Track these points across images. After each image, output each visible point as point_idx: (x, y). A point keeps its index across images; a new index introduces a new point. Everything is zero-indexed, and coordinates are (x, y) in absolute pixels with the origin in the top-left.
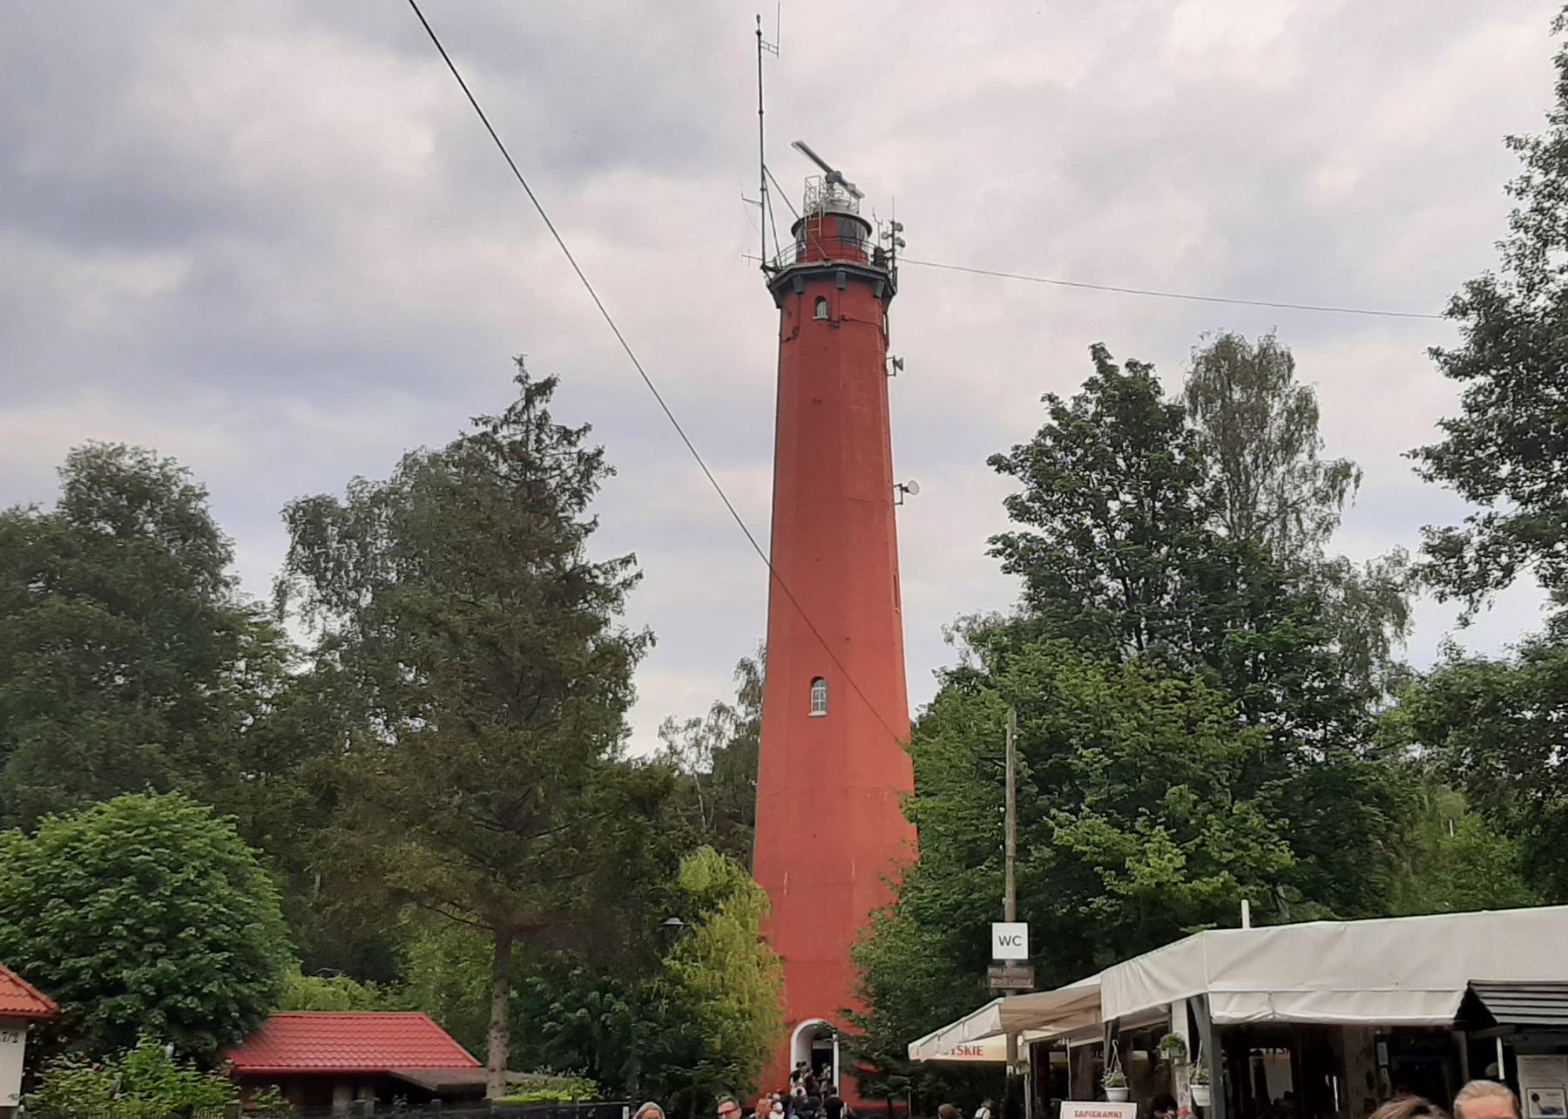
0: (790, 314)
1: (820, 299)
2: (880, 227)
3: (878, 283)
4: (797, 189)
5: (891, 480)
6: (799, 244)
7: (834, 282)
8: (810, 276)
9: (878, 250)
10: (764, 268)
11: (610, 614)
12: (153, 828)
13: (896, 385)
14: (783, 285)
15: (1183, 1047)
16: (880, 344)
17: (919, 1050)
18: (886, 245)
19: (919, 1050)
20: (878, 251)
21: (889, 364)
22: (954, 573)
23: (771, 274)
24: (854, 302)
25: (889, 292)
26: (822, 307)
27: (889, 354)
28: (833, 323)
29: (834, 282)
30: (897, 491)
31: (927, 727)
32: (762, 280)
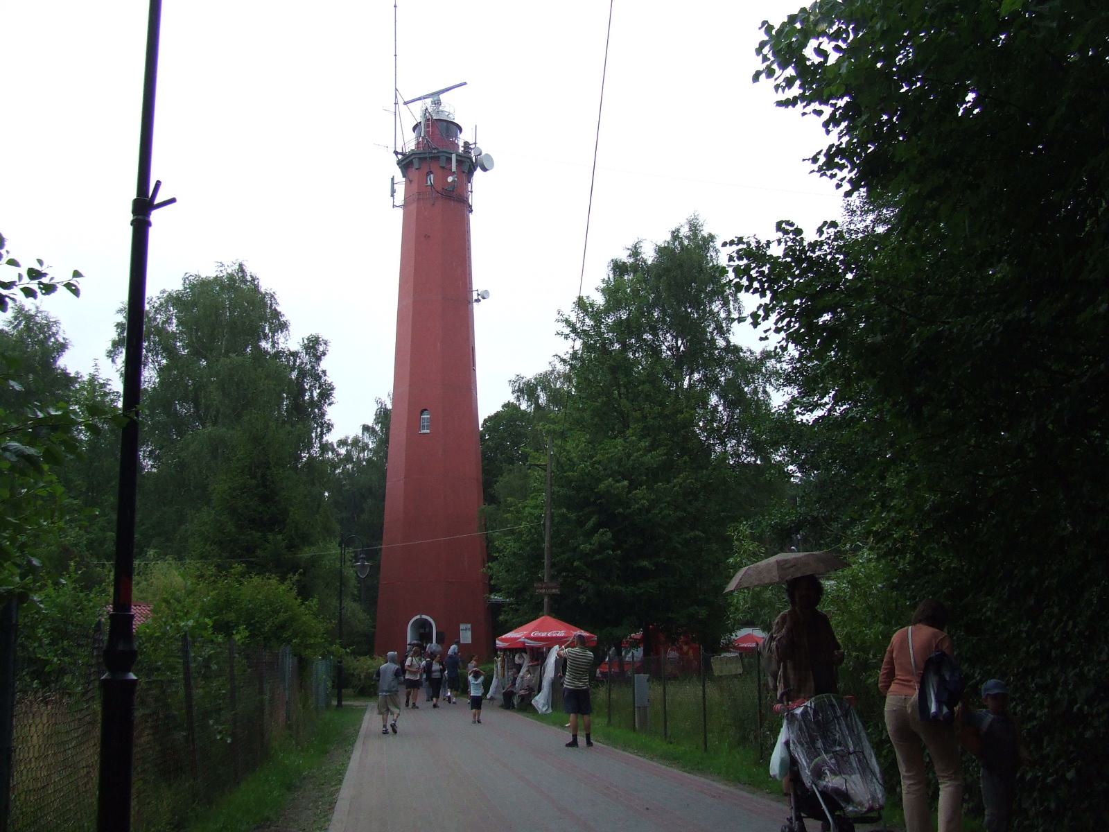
0: (411, 181)
4: (415, 114)
5: (471, 288)
6: (418, 137)
7: (439, 169)
10: (396, 153)
23: (400, 157)
29: (439, 169)
32: (394, 159)
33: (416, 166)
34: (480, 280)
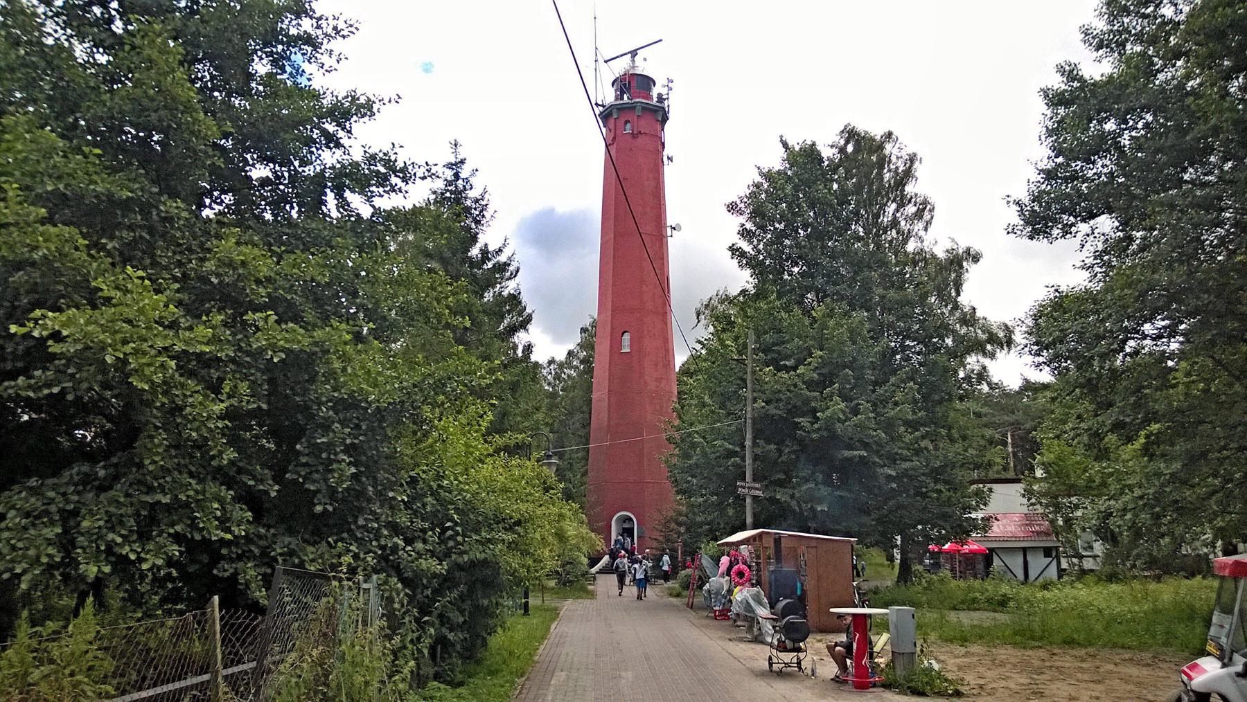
1: (627, 122)
2: (660, 81)
3: (660, 114)
7: (634, 118)
8: (621, 109)
9: (660, 96)
11: (510, 287)
12: (1036, 663)
13: (674, 244)
14: (607, 115)
15: (760, 535)
16: (660, 147)
17: (832, 610)
18: (664, 91)
19: (832, 610)
20: (660, 96)
21: (665, 159)
22: (706, 251)
24: (645, 124)
25: (665, 119)
26: (628, 126)
27: (665, 153)
28: (634, 135)
29: (634, 118)
30: (669, 230)
31: (686, 371)
33: (615, 116)
34: (673, 213)
